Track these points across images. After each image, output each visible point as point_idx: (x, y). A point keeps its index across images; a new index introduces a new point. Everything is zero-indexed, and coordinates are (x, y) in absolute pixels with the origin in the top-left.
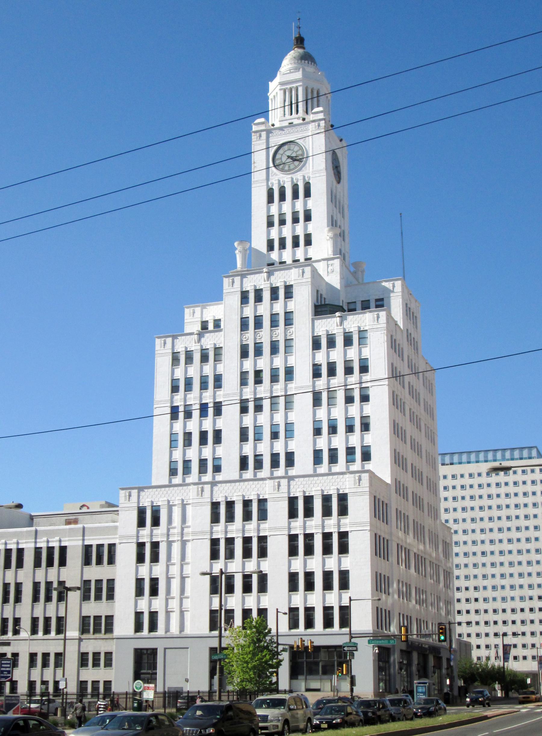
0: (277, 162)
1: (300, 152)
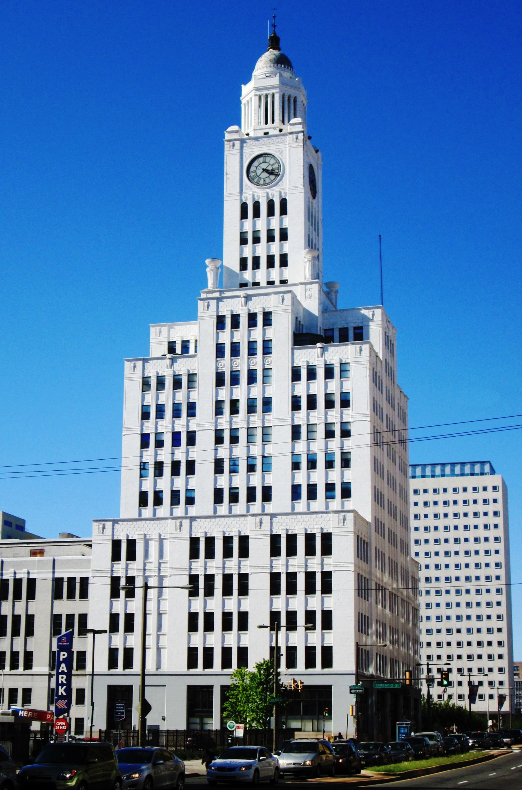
0: (252, 175)
1: (276, 166)
